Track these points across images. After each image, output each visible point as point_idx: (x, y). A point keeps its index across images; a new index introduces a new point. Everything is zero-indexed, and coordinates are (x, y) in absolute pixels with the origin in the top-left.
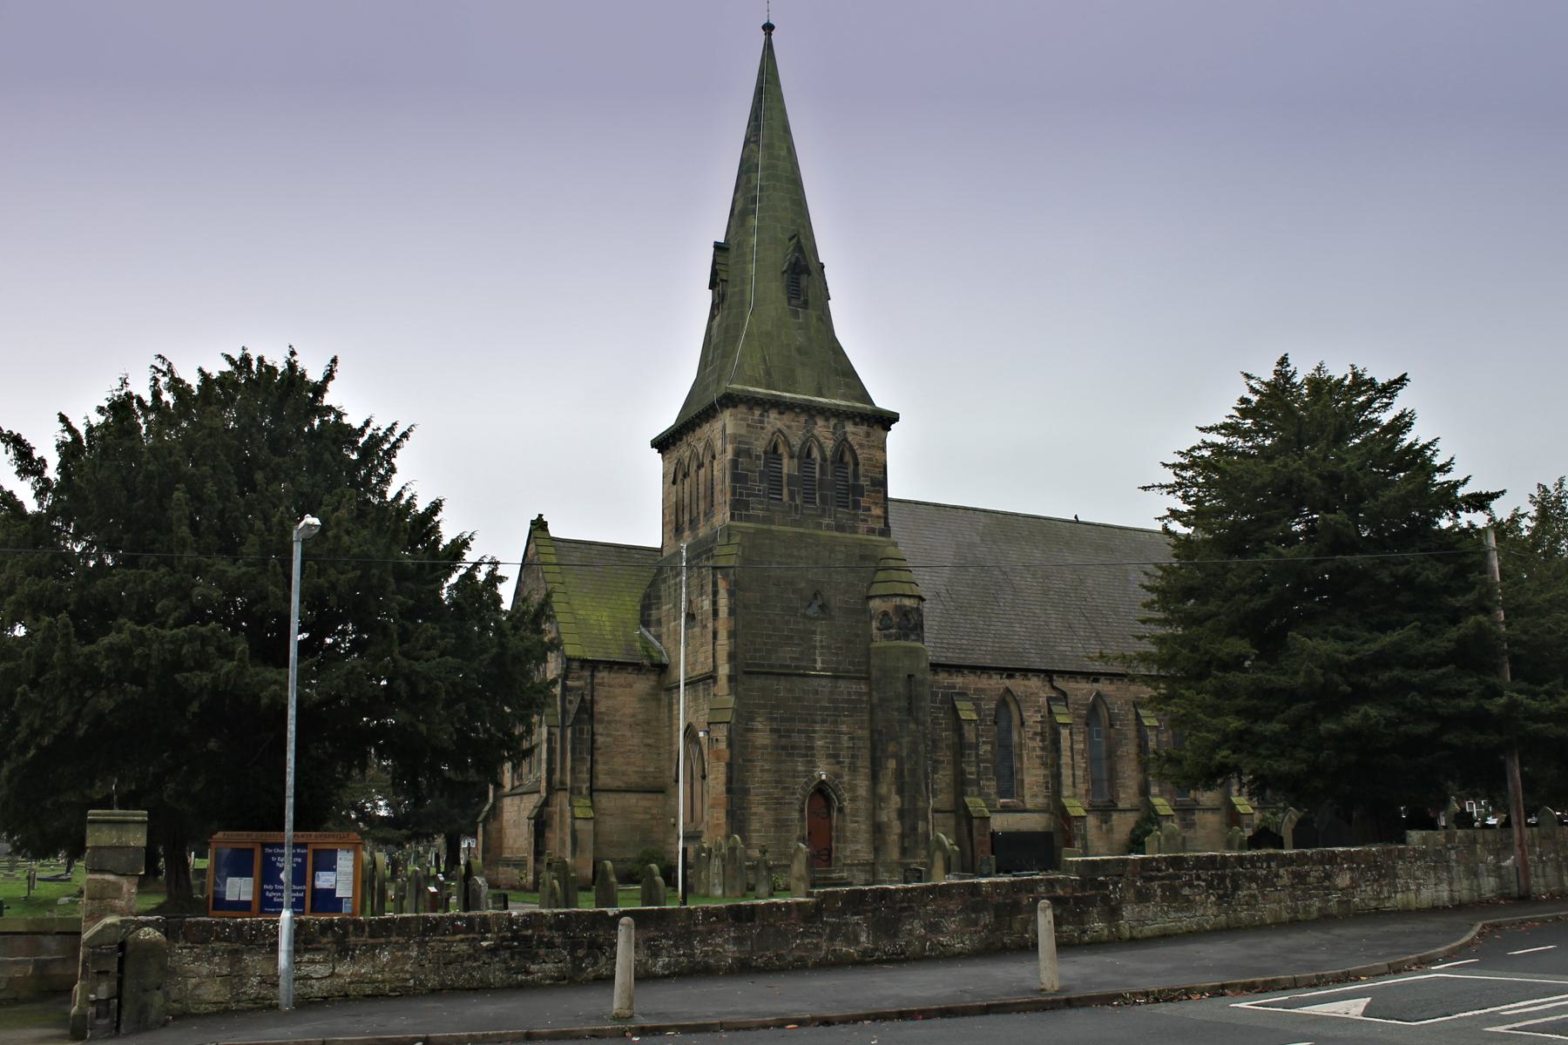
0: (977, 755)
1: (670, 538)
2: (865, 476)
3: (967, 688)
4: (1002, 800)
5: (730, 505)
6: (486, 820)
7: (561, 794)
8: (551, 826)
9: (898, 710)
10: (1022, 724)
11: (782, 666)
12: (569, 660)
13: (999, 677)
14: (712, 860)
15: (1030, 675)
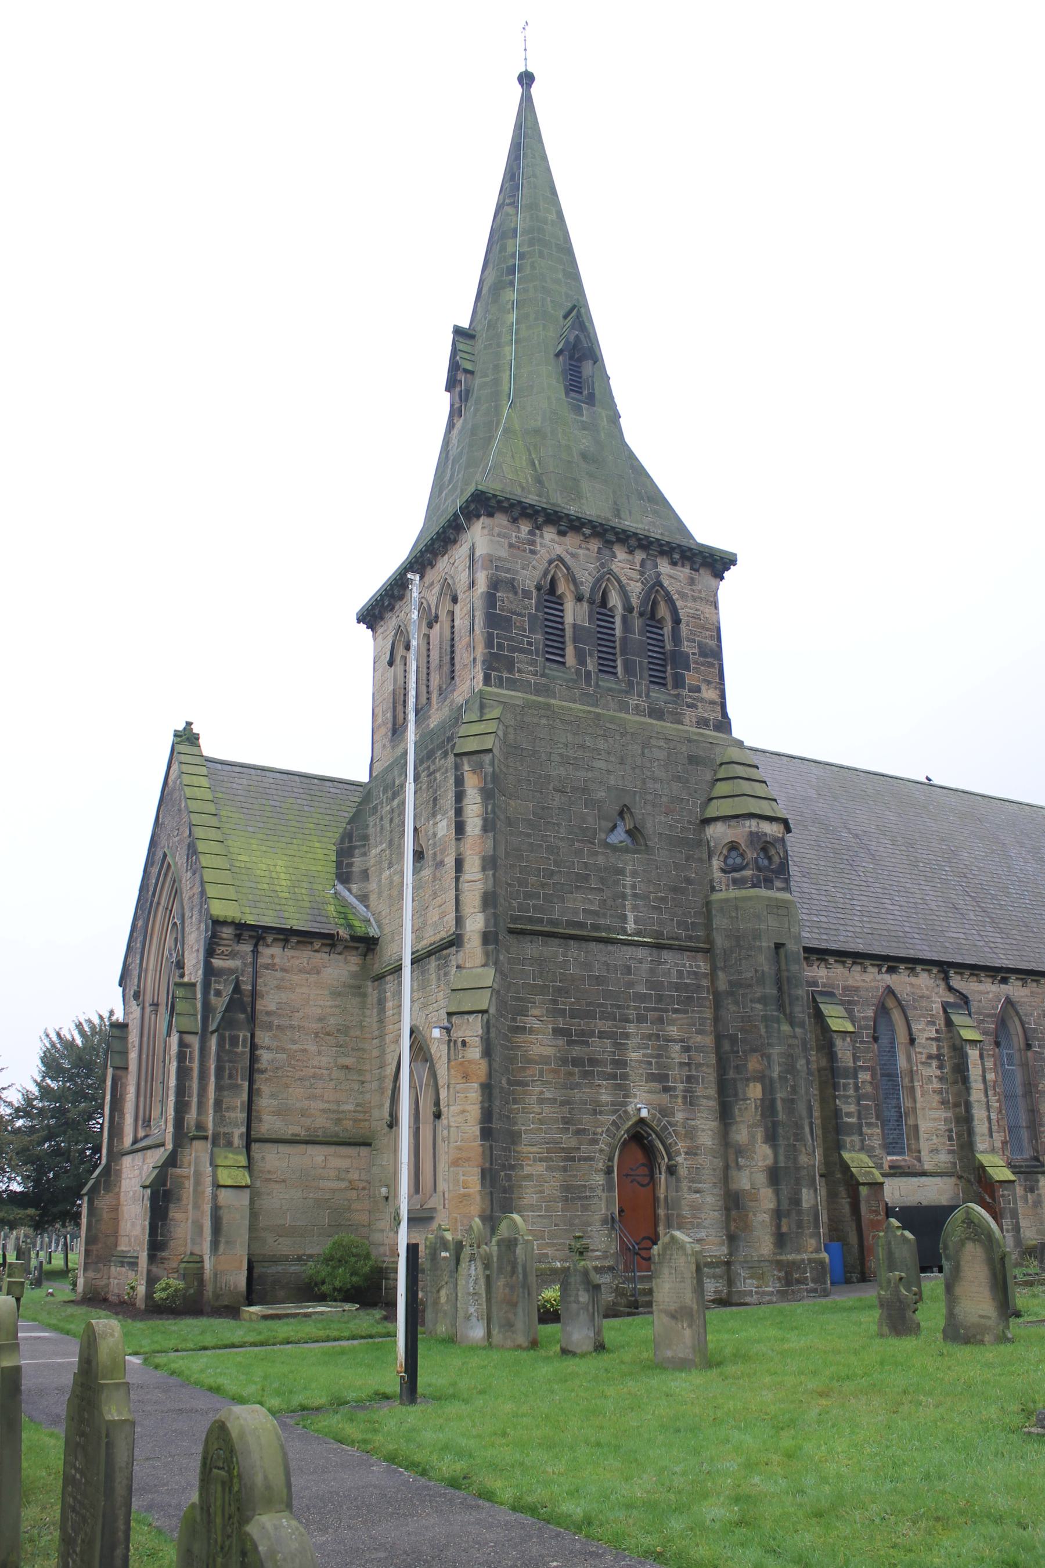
0: (857, 1088)
1: (384, 746)
2: (689, 640)
3: (832, 986)
4: (889, 1158)
5: (484, 662)
6: (94, 1190)
7: (197, 1144)
8: (179, 1200)
9: (763, 1000)
10: (912, 1041)
11: (571, 924)
12: (217, 923)
13: (875, 970)
14: (464, 1265)
15: (919, 968)
